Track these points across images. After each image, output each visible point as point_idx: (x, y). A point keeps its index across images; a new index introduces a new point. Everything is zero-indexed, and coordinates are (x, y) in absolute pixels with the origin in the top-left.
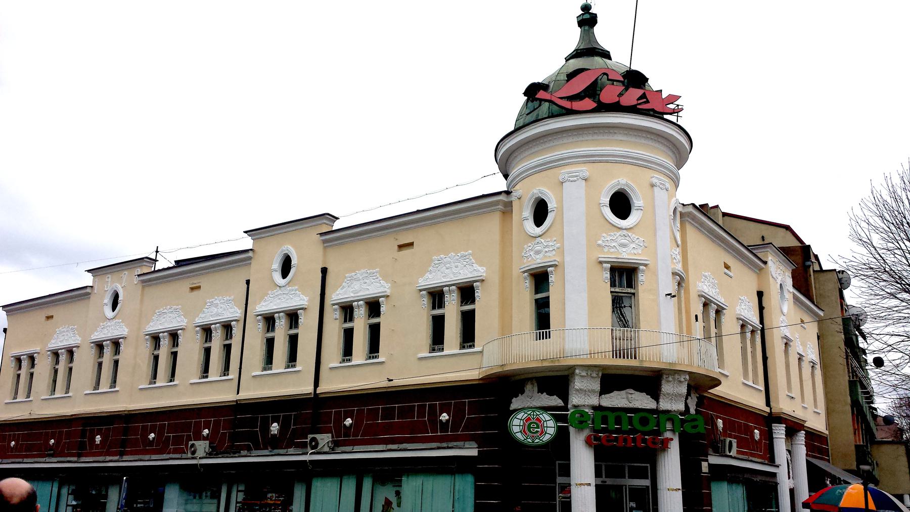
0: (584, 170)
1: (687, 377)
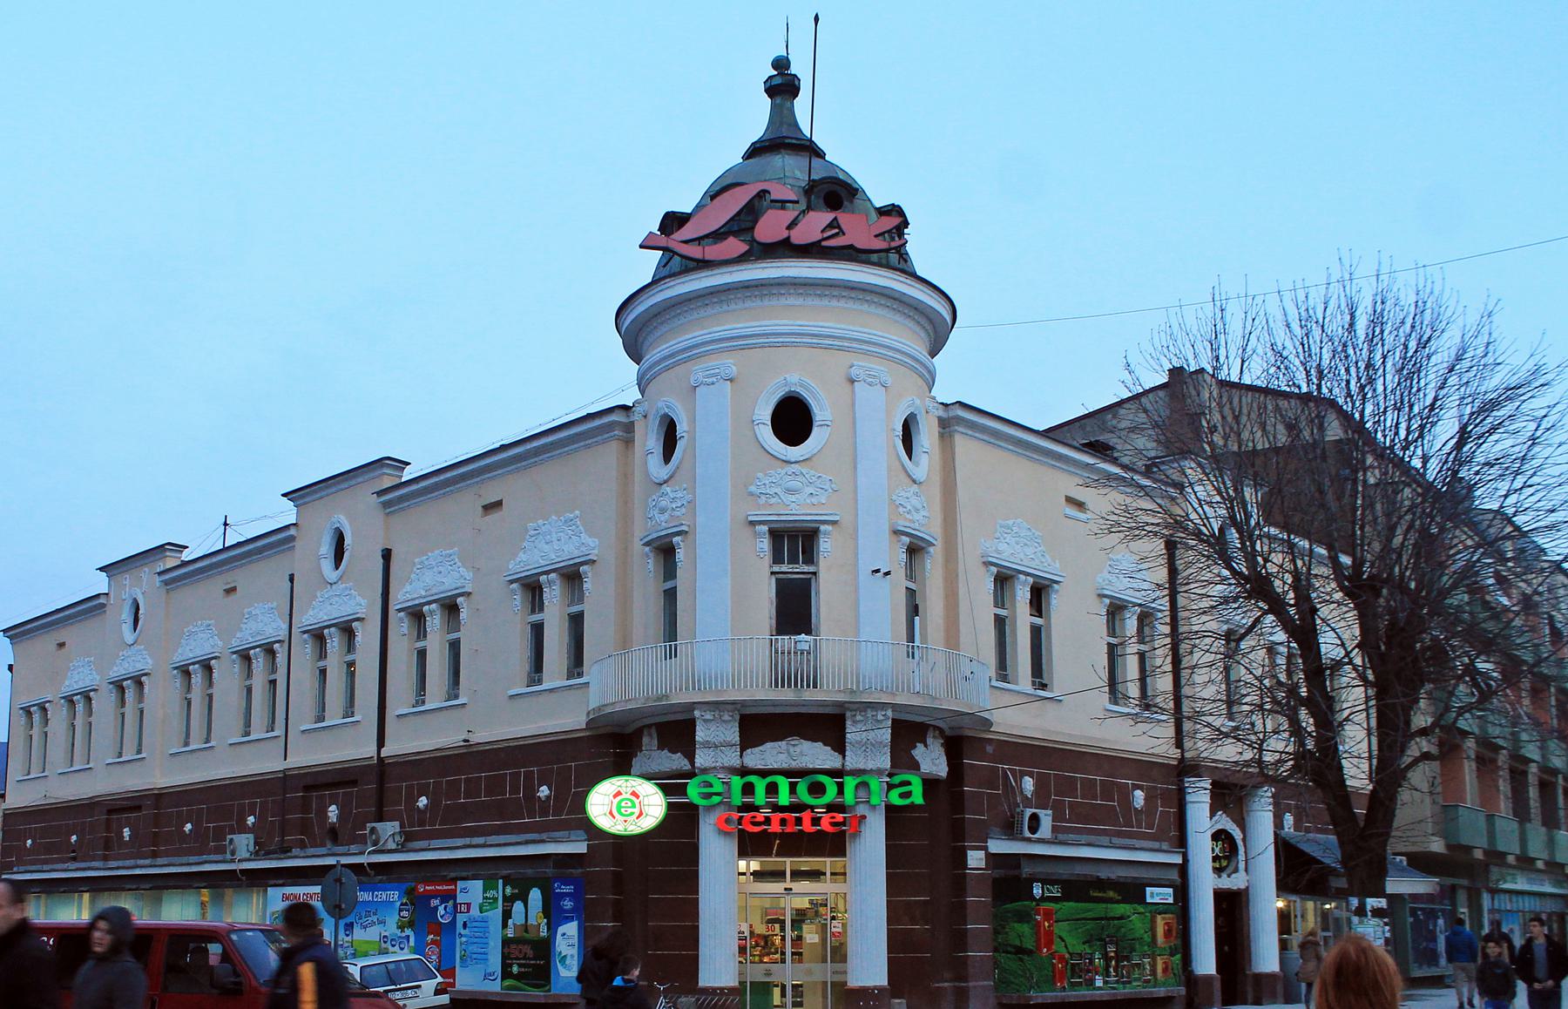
0: (729, 364)
1: (889, 713)
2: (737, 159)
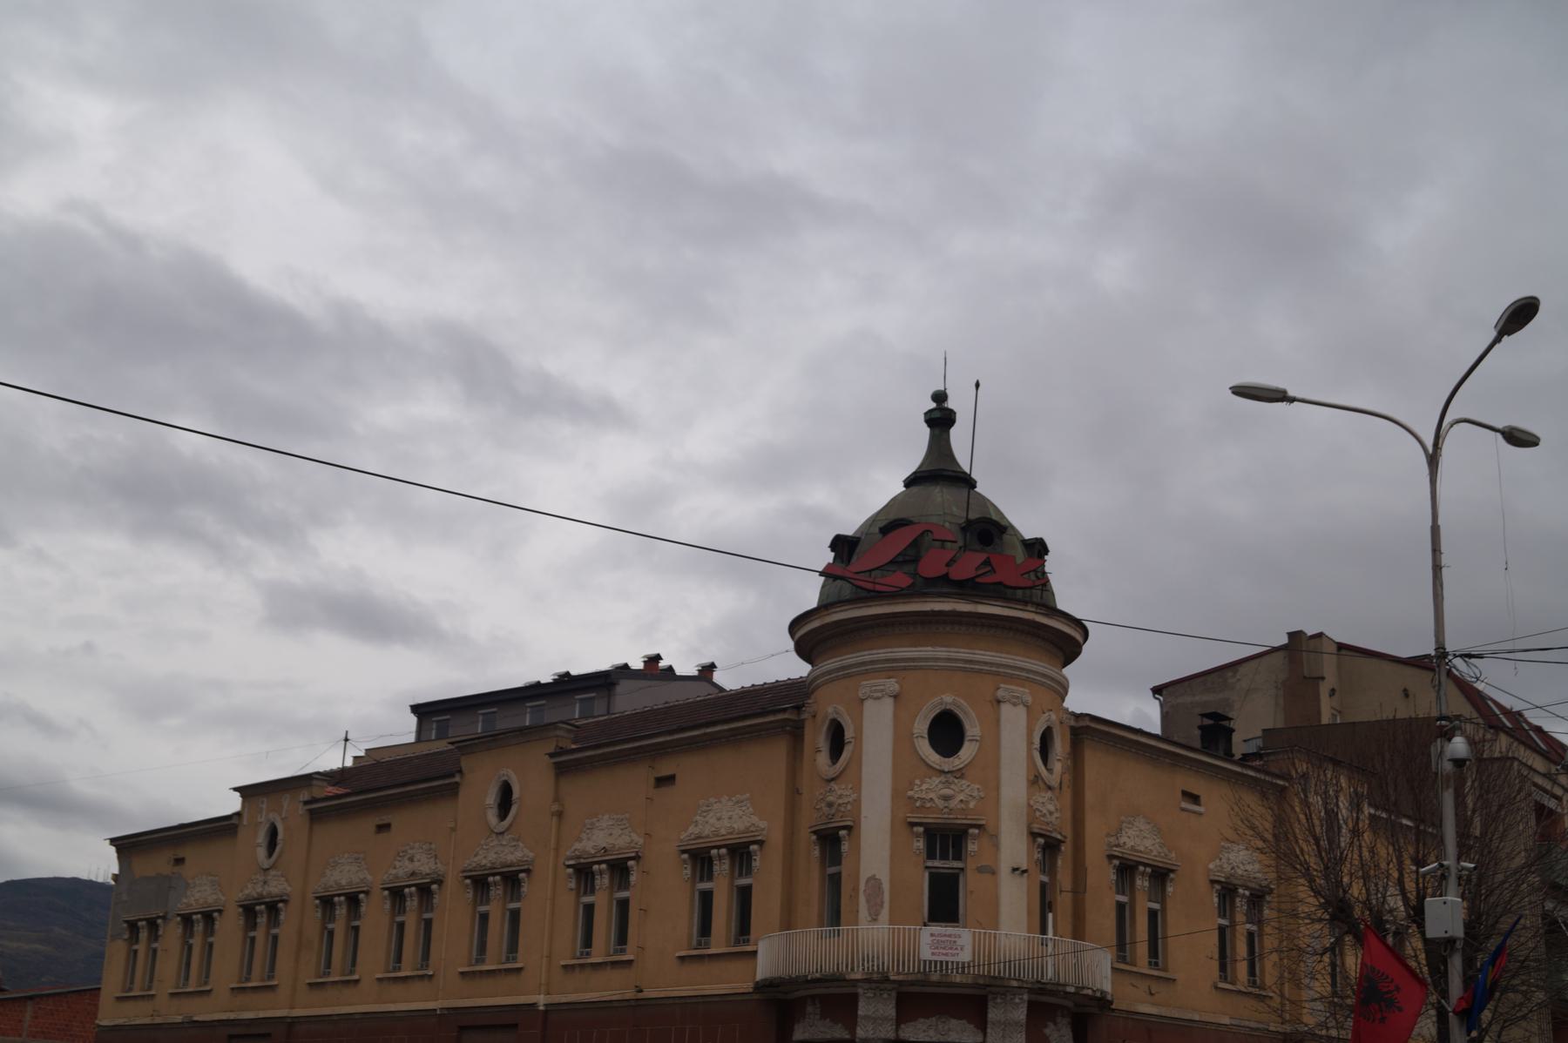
2: (899, 488)
